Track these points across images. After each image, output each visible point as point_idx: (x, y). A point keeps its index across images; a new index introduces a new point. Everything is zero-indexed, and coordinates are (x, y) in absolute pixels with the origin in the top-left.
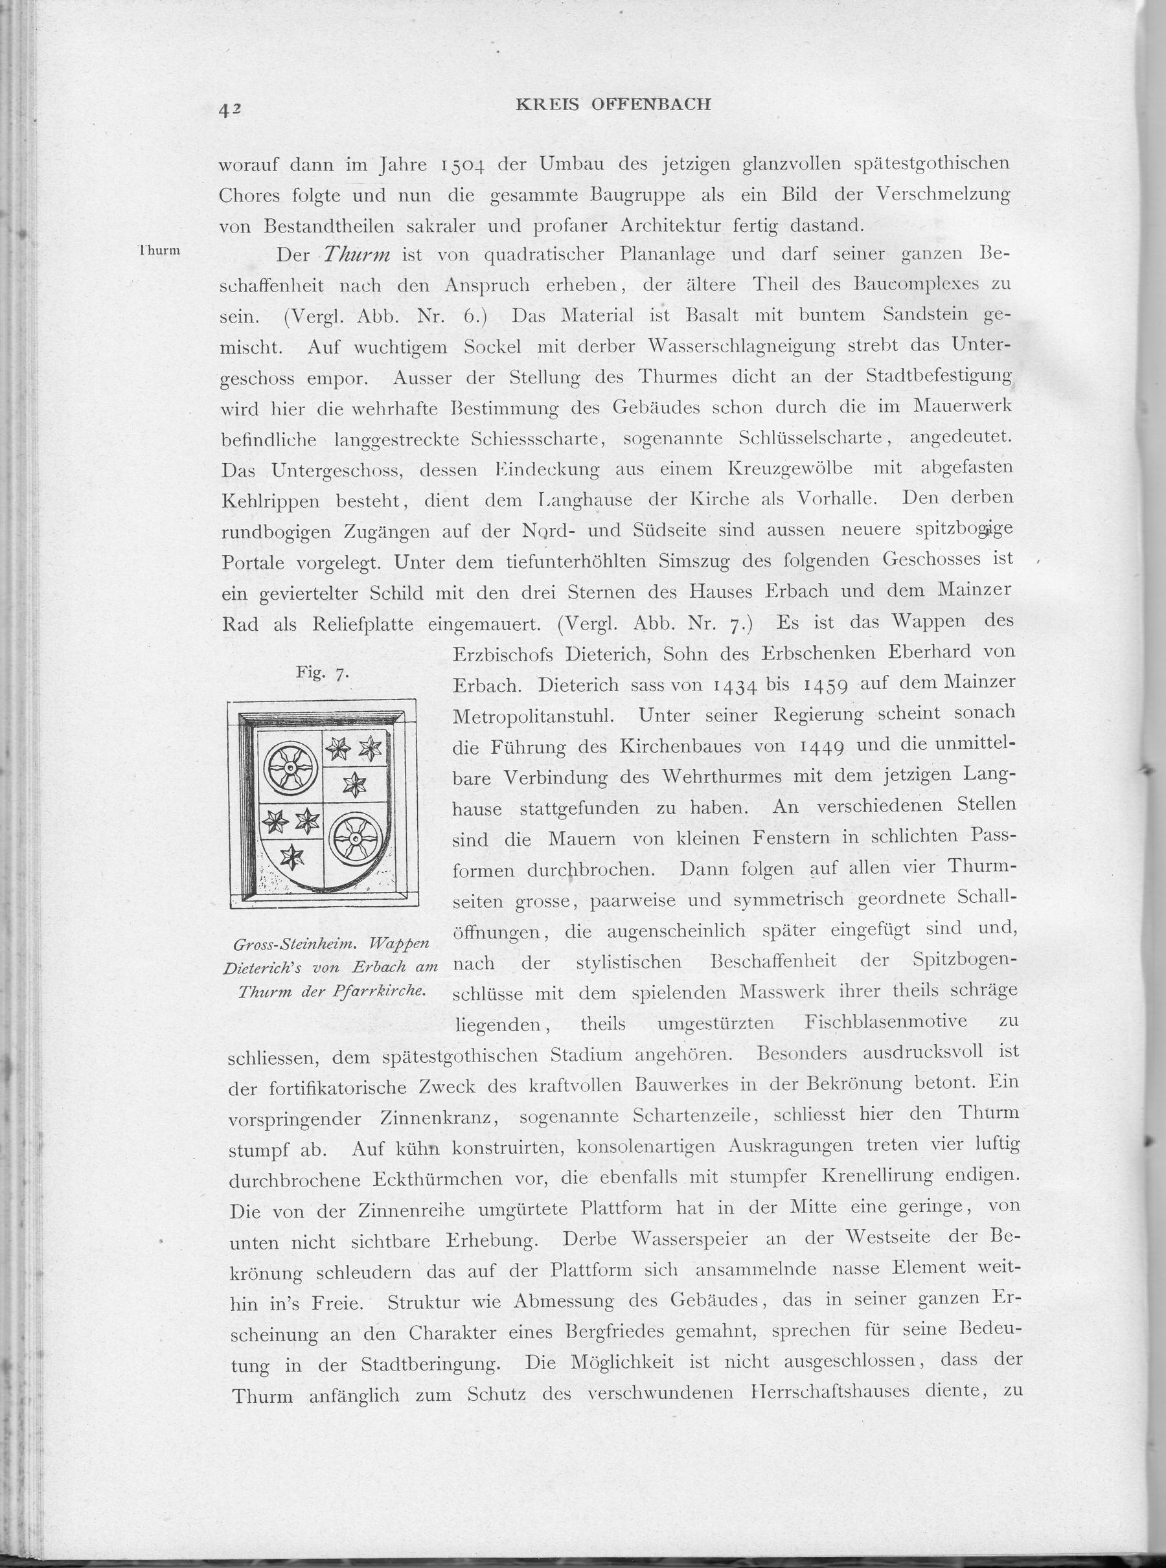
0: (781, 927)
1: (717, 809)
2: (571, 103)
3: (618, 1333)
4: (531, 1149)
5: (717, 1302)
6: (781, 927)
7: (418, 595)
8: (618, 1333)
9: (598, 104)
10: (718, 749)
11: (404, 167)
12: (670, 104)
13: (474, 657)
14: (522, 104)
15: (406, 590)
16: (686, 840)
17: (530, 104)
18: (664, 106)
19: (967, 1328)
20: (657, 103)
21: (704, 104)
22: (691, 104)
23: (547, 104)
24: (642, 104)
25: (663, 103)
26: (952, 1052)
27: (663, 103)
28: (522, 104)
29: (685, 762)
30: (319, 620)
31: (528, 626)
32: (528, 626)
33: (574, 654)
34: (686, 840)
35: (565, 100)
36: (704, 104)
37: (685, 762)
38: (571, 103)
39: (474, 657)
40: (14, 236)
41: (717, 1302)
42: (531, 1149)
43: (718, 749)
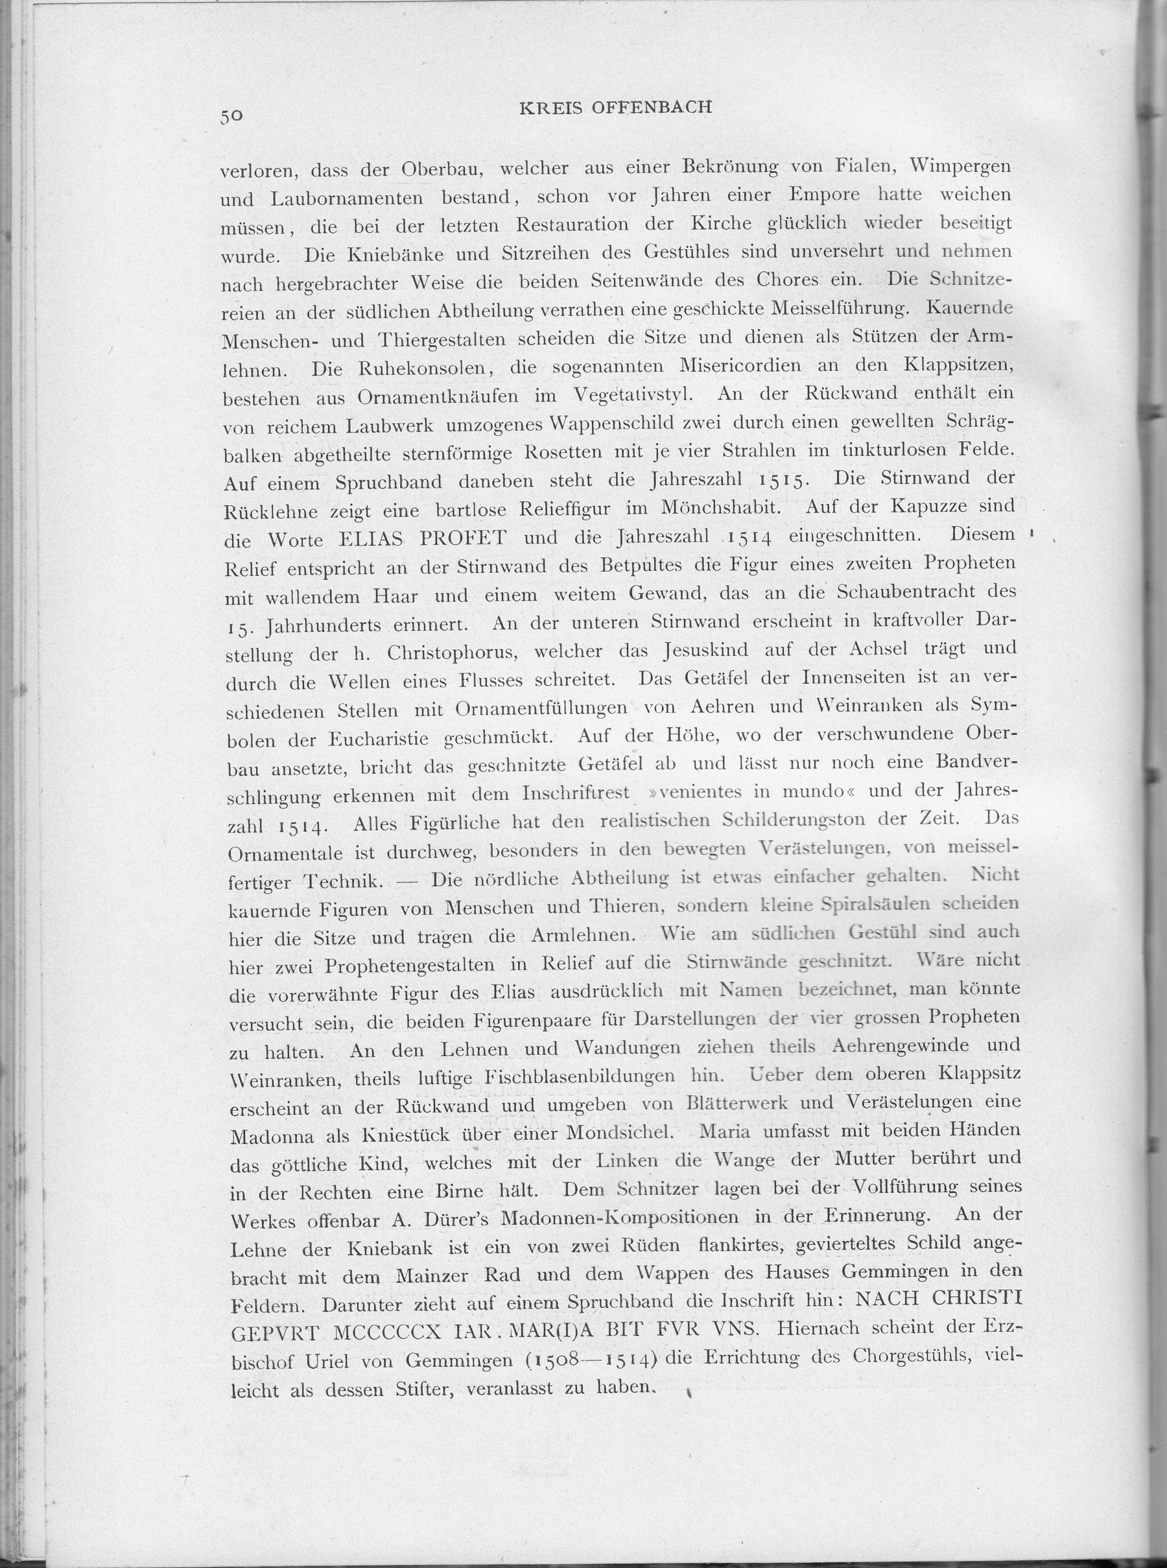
0: (401, 252)
1: (624, 1388)
2: (572, 107)
3: (327, 1364)
4: (754, 1247)
5: (480, 398)
6: (401, 252)
7: (955, 1244)
8: (327, 1364)
9: (598, 107)
10: (957, 310)
11: (979, 792)
12: (671, 107)
13: (1005, 1328)
14: (525, 109)
15: (944, 1239)
16: (269, 514)
17: (534, 108)
18: (665, 109)
19: (943, 761)
20: (658, 105)
21: (705, 106)
22: (692, 106)
23: (551, 108)
24: (643, 107)
25: (664, 106)
26: (391, 539)
27: (664, 106)
28: (525, 109)
29: (840, 692)
30: (306, 1189)
31: (455, 626)
32: (455, 626)
33: (896, 278)
34: (269, 514)
35: (568, 103)
36: (705, 106)
37: (840, 692)
38: (572, 107)
39: (1005, 1328)
40: (4, 237)
41: (480, 398)
42: (754, 1247)
43: (957, 310)
